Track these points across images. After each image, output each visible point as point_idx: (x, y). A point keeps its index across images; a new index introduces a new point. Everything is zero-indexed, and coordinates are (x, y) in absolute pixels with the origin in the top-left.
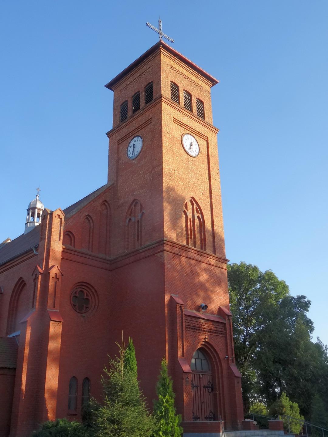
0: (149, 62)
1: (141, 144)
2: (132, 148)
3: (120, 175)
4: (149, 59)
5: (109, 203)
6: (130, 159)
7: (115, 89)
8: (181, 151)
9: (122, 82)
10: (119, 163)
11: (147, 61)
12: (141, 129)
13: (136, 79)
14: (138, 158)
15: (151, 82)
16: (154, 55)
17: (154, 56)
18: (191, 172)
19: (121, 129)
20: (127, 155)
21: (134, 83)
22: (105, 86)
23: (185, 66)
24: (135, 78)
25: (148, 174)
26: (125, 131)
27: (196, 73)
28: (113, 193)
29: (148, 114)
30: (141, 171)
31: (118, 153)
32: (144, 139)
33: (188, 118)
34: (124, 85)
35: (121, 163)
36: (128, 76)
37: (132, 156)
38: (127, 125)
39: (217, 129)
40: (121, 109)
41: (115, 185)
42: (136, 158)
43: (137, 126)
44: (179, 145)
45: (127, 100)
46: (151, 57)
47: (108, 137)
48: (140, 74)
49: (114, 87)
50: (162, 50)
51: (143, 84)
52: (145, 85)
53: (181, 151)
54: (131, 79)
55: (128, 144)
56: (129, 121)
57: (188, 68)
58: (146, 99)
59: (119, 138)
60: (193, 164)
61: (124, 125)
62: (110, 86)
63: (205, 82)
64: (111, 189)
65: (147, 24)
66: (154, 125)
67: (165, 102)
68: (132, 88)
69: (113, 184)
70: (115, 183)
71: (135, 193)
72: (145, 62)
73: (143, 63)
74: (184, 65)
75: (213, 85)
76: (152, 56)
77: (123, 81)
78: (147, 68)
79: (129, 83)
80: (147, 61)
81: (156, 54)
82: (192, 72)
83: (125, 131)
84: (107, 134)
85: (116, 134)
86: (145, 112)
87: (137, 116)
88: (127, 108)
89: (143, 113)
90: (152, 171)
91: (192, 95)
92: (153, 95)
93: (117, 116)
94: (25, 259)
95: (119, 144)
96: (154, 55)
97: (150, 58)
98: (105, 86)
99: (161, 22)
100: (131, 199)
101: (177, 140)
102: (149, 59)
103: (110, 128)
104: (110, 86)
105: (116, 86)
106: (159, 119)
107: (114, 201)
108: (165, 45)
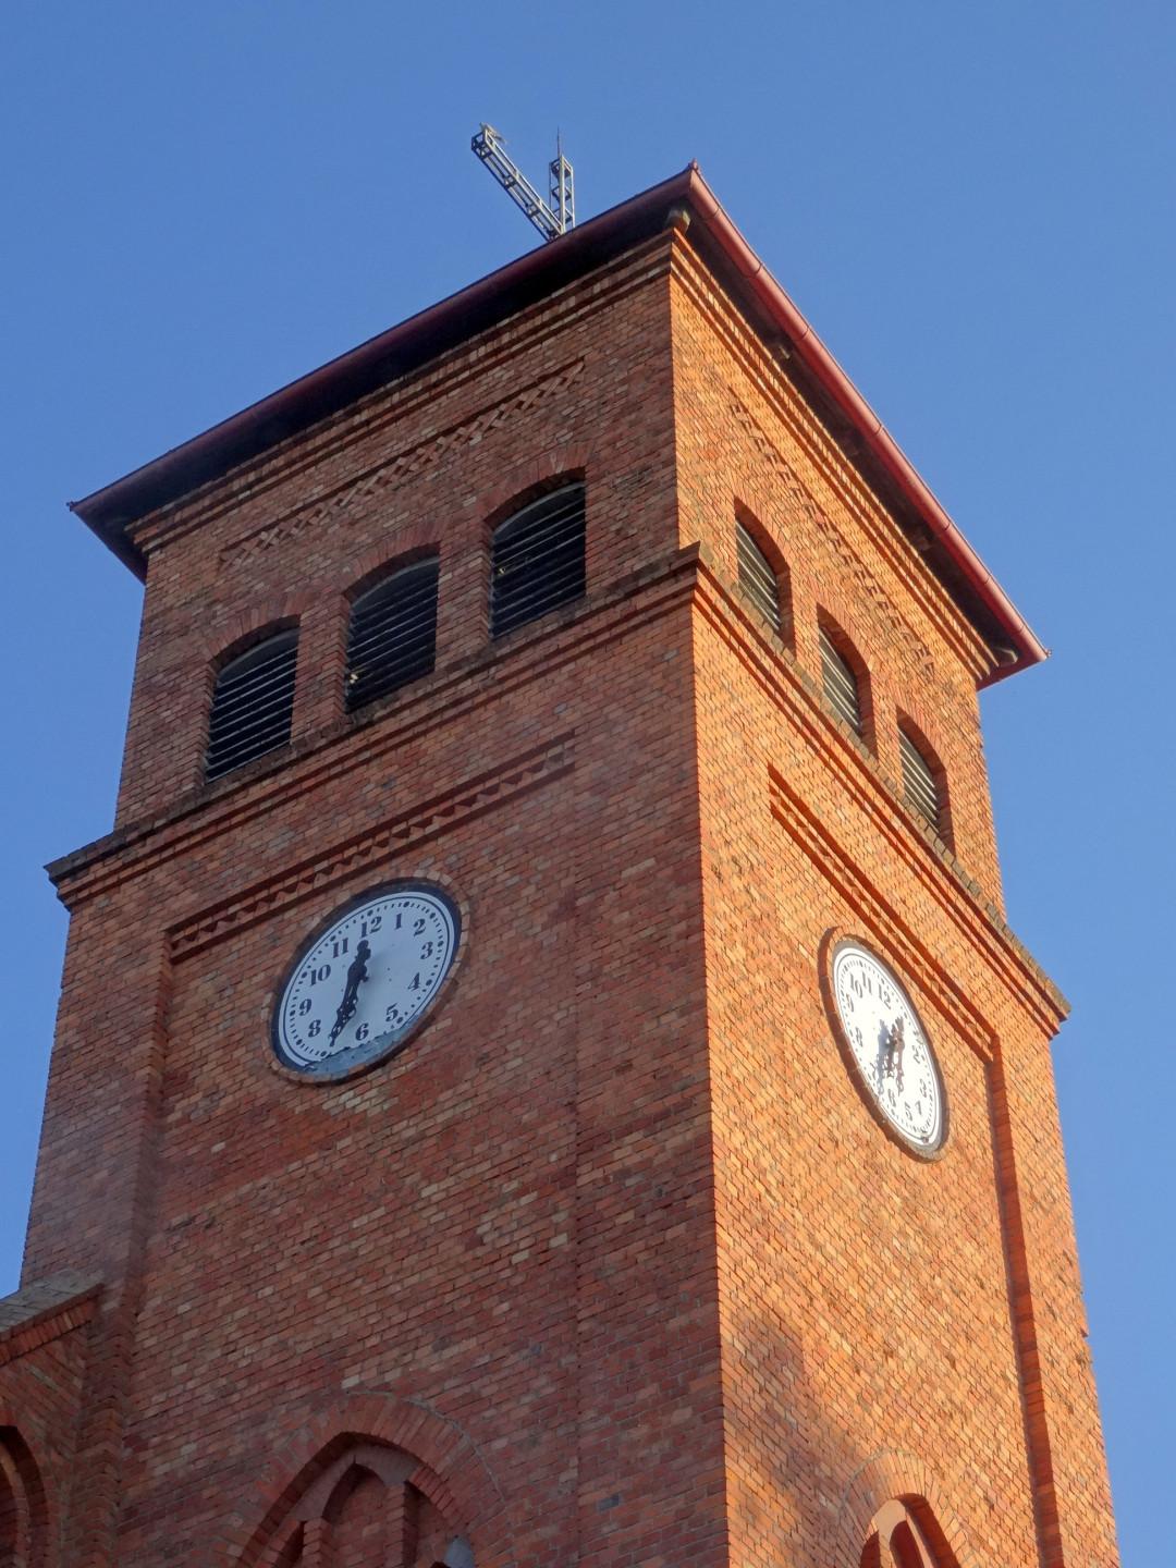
0: (540, 341)
1: (442, 955)
2: (340, 978)
3: (176, 1221)
4: (547, 316)
5: (41, 1458)
6: (310, 1078)
7: (161, 546)
8: (826, 1065)
9: (250, 486)
10: (172, 1118)
11: (523, 329)
12: (444, 830)
13: (401, 461)
14: (403, 1066)
15: (565, 474)
16: (597, 288)
17: (603, 293)
18: (896, 1272)
19: (222, 826)
20: (276, 1045)
21: (369, 492)
22: (72, 506)
23: (826, 442)
24: (386, 453)
25: (524, 1200)
26: (268, 842)
27: (892, 531)
28: (78, 1383)
29: (528, 704)
30: (429, 1178)
31: (162, 1028)
32: (482, 911)
33: (866, 819)
34: (272, 505)
35: (186, 1119)
36: (319, 441)
37: (334, 1050)
38: (287, 795)
39: (1054, 990)
40: (218, 692)
41: (110, 1305)
42: (381, 1063)
43: (406, 799)
44: (802, 998)
45: (297, 617)
46: (572, 302)
47: (62, 898)
48: (444, 424)
49: (163, 525)
50: (683, 256)
51: (473, 491)
52: (498, 502)
53: (826, 1065)
54: (345, 465)
55: (288, 956)
56: (313, 764)
57: (844, 466)
58: (496, 606)
59: (187, 901)
60: (910, 1211)
61: (256, 792)
62: (126, 518)
63: (946, 622)
64: (63, 1336)
65: (478, 145)
66: (599, 787)
67: (718, 623)
68: (352, 524)
69: (96, 1296)
70: (117, 1285)
71: (350, 1382)
72: (506, 338)
73: (484, 341)
74: (820, 434)
75: (998, 674)
76: (574, 292)
77: (259, 480)
78: (525, 380)
79: (319, 491)
80: (523, 329)
81: (622, 274)
82: (863, 511)
83: (268, 842)
84: (61, 873)
85: (159, 875)
86: (497, 690)
87: (407, 717)
88: (292, 688)
89: (477, 693)
90: (576, 1165)
91: (867, 673)
92: (590, 568)
93: (176, 740)
94: (752, 351)
95: (175, 961)
96: (597, 288)
97: (562, 308)
98: (72, 506)
99: (567, 174)
100: (298, 1434)
101: (796, 959)
102: (547, 316)
103: (100, 823)
104: (126, 518)
105: (178, 517)
106: (668, 732)
107: (89, 1453)
108: (712, 216)
